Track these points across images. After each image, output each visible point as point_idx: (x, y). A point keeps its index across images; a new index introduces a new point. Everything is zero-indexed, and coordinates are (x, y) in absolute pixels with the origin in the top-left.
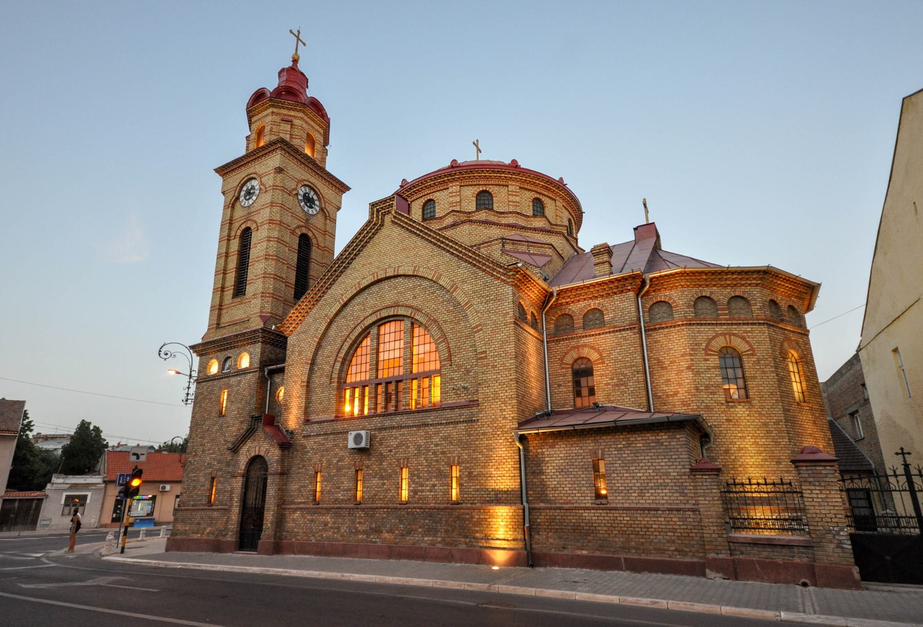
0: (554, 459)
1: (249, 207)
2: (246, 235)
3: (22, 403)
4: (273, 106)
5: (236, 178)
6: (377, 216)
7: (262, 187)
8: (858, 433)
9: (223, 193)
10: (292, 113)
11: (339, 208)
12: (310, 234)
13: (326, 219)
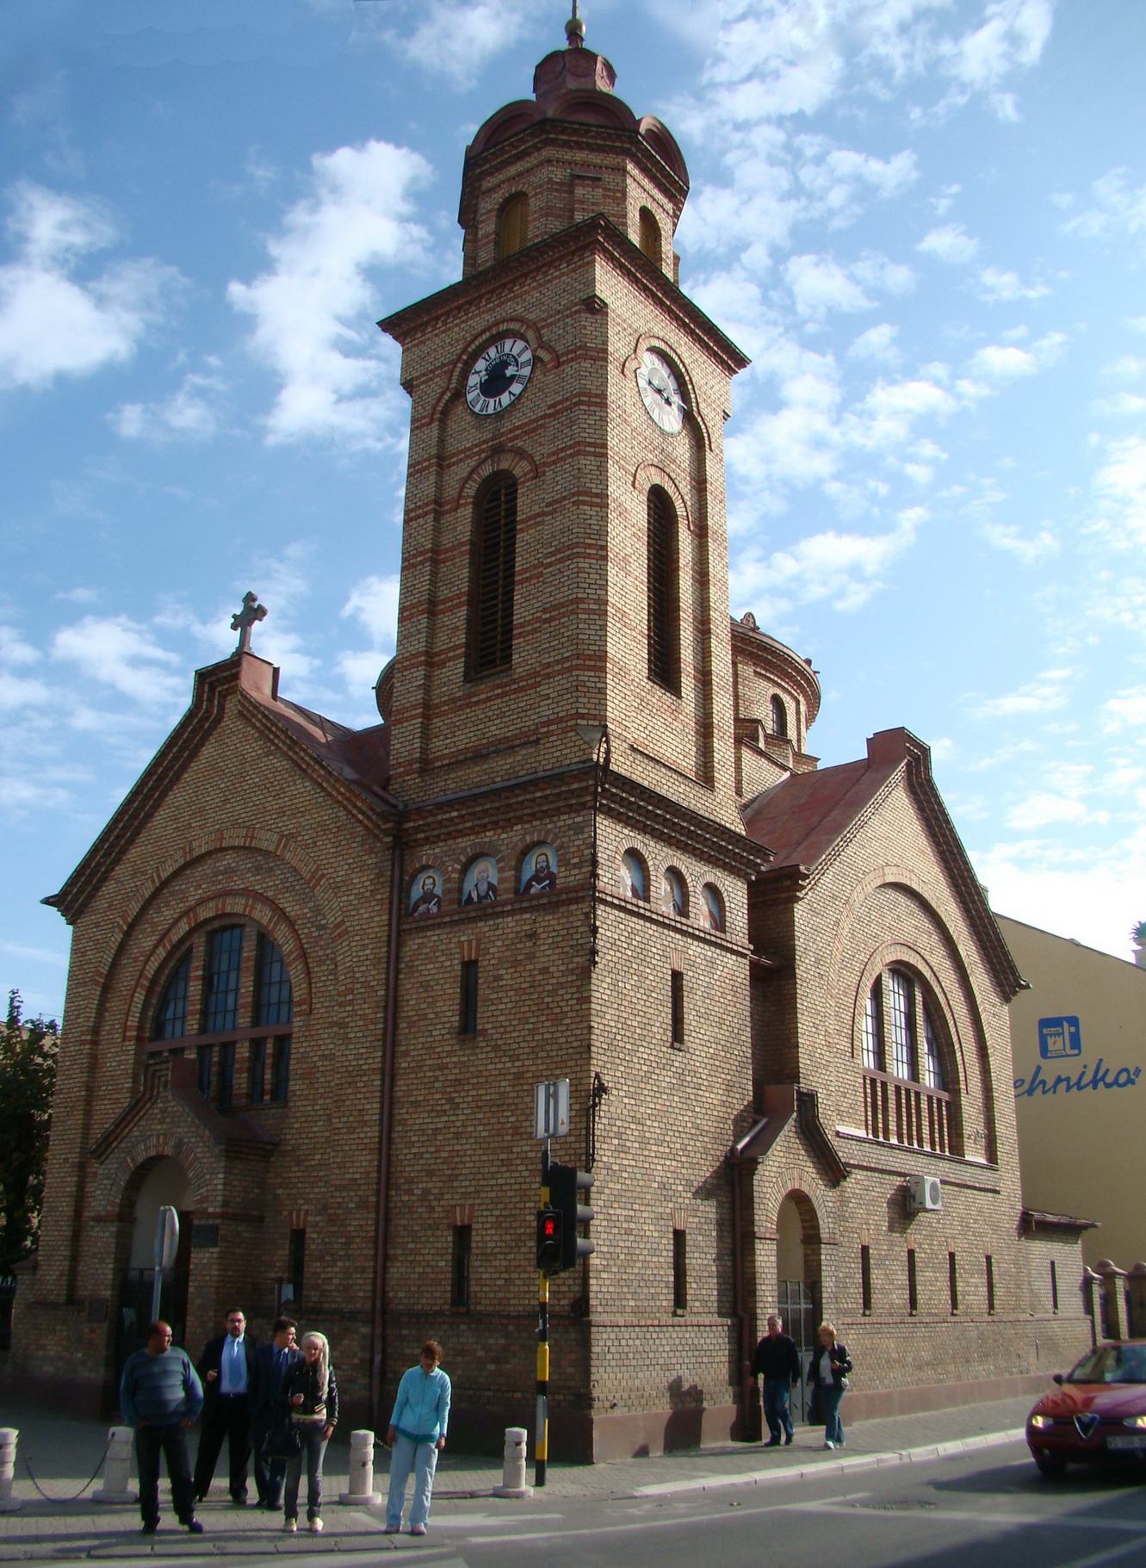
1: (499, 416)
2: (664, 670)
3: (868, 740)
5: (446, 342)
6: (210, 700)
7: (542, 354)
8: (157, 1243)
9: (408, 385)
12: (670, 490)
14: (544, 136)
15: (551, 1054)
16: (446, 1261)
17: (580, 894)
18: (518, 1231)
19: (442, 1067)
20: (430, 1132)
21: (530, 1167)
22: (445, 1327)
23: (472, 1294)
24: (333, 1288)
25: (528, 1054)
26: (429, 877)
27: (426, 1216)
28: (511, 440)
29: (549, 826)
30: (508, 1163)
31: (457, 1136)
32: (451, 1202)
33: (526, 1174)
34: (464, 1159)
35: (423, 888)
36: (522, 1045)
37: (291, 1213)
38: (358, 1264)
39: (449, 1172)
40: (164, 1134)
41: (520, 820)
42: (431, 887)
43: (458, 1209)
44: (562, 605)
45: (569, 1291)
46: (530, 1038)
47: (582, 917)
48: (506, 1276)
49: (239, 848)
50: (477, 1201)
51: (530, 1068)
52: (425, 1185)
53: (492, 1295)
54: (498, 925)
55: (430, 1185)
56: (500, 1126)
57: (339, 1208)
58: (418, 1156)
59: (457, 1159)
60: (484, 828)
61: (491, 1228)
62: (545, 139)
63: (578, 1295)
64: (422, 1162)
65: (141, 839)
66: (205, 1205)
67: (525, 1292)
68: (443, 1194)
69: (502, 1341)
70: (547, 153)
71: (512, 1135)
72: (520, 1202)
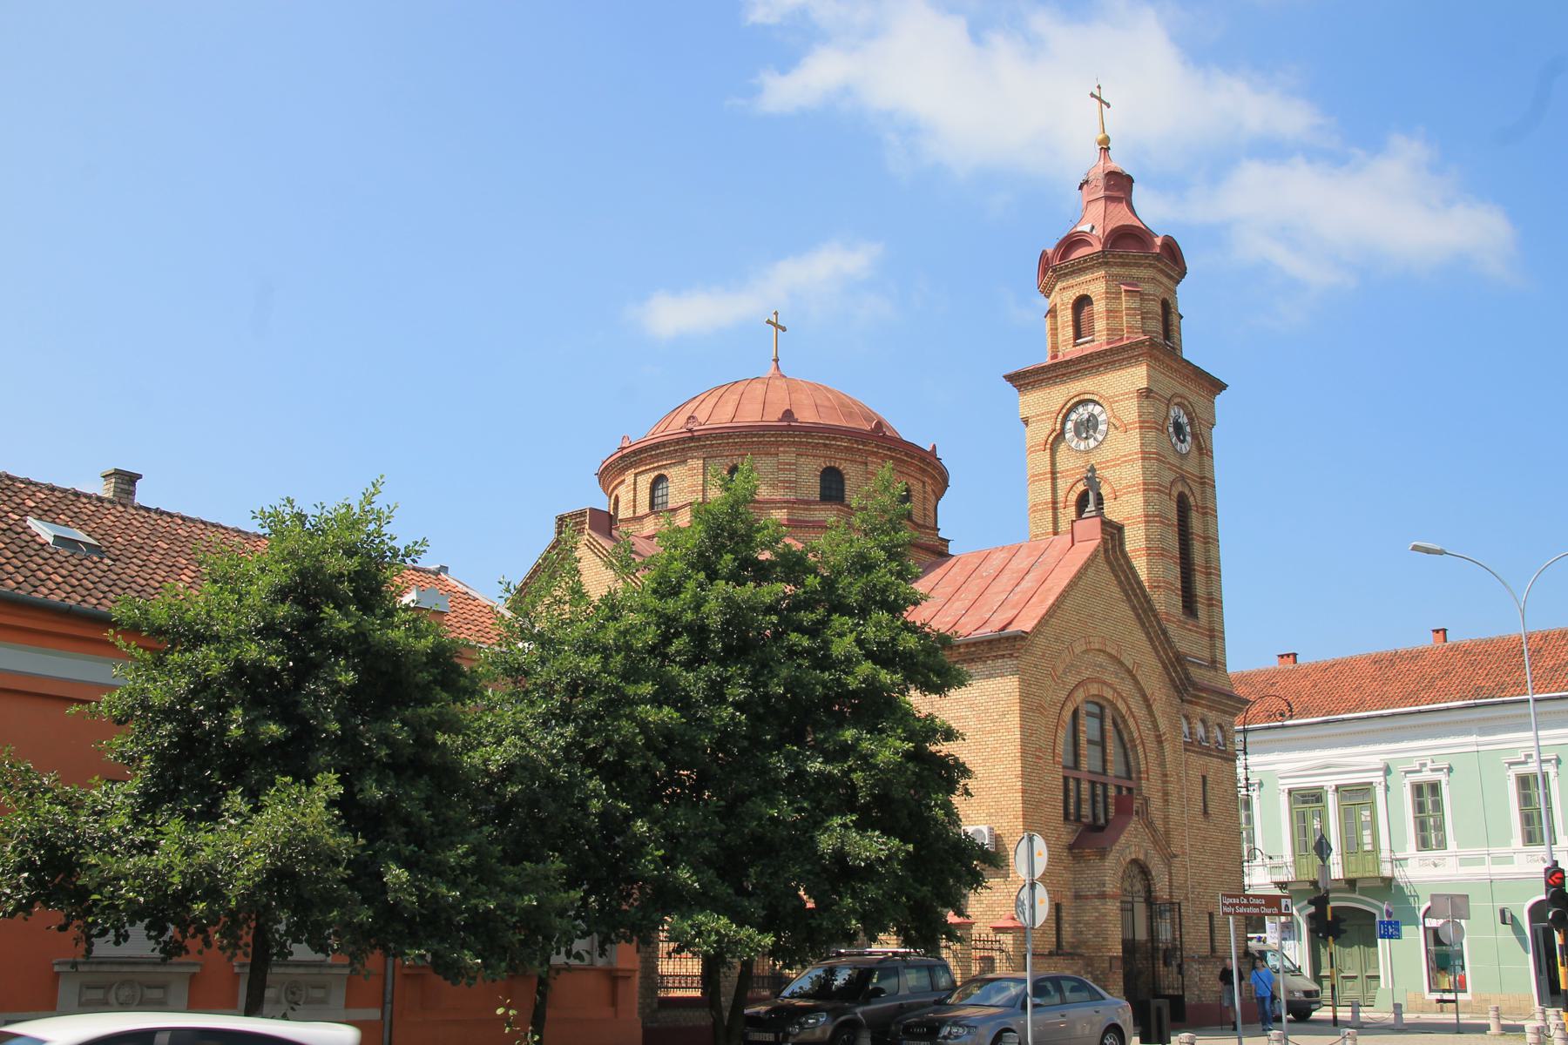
4: (1106, 263)
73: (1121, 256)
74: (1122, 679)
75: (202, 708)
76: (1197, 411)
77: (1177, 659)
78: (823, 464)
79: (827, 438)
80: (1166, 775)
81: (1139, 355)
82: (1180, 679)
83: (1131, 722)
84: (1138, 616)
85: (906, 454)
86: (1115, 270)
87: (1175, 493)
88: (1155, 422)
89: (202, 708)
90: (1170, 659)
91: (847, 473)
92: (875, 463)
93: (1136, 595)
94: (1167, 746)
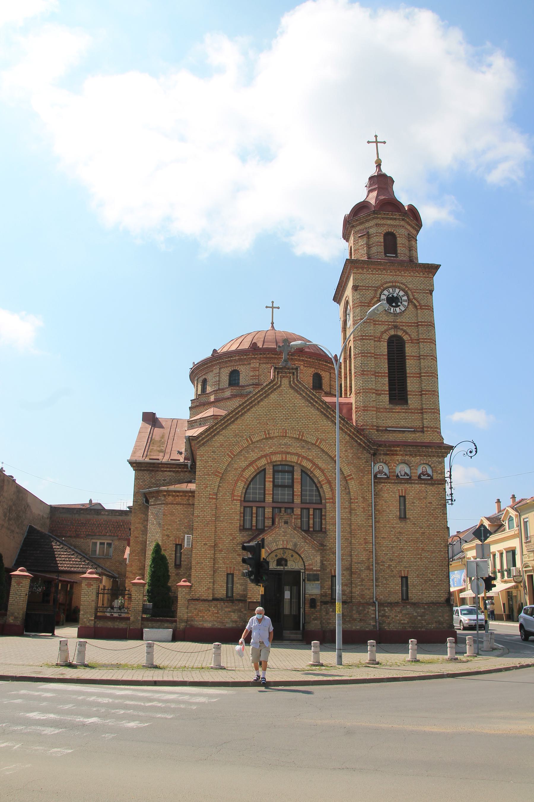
0: (209, 573)
4: (353, 226)
10: (367, 225)
11: (431, 292)
12: (400, 333)
13: (417, 309)
14: (403, 218)
15: (434, 528)
16: (399, 587)
17: (442, 482)
18: (425, 579)
19: (394, 528)
20: (390, 547)
21: (428, 560)
22: (402, 607)
23: (410, 597)
24: (357, 595)
25: (426, 527)
26: (381, 465)
27: (391, 573)
28: (401, 326)
29: (430, 460)
30: (421, 559)
31: (401, 549)
32: (400, 569)
33: (427, 562)
34: (404, 556)
35: (379, 468)
36: (424, 524)
37: (331, 570)
38: (367, 587)
39: (399, 560)
40: (286, 541)
41: (420, 456)
42: (382, 469)
43: (403, 571)
44: (429, 391)
45: (444, 596)
46: (426, 522)
47: (443, 489)
48: (422, 592)
49: (295, 438)
50: (410, 569)
51: (427, 531)
52: (389, 564)
53: (417, 597)
54: (413, 486)
55: (391, 564)
56: (417, 548)
57: (357, 569)
58: (385, 554)
59: (402, 556)
60: (406, 455)
61: (415, 577)
62: (404, 219)
63: (447, 597)
64: (387, 556)
65: (239, 421)
66: (311, 567)
67: (429, 596)
68: (396, 567)
69: (423, 610)
70: (402, 223)
71: (422, 550)
72: (426, 570)
73: (357, 220)
74: (309, 449)
75: (159, 498)
76: (409, 286)
77: (358, 432)
78: (230, 369)
79: (228, 357)
80: (351, 499)
81: (350, 270)
82: (364, 443)
83: (317, 473)
84: (321, 412)
85: (273, 354)
86: (358, 228)
87: (386, 337)
88: (360, 303)
89: (159, 498)
90: (353, 434)
91: (241, 370)
92: (255, 362)
93: (316, 402)
94: (352, 484)
